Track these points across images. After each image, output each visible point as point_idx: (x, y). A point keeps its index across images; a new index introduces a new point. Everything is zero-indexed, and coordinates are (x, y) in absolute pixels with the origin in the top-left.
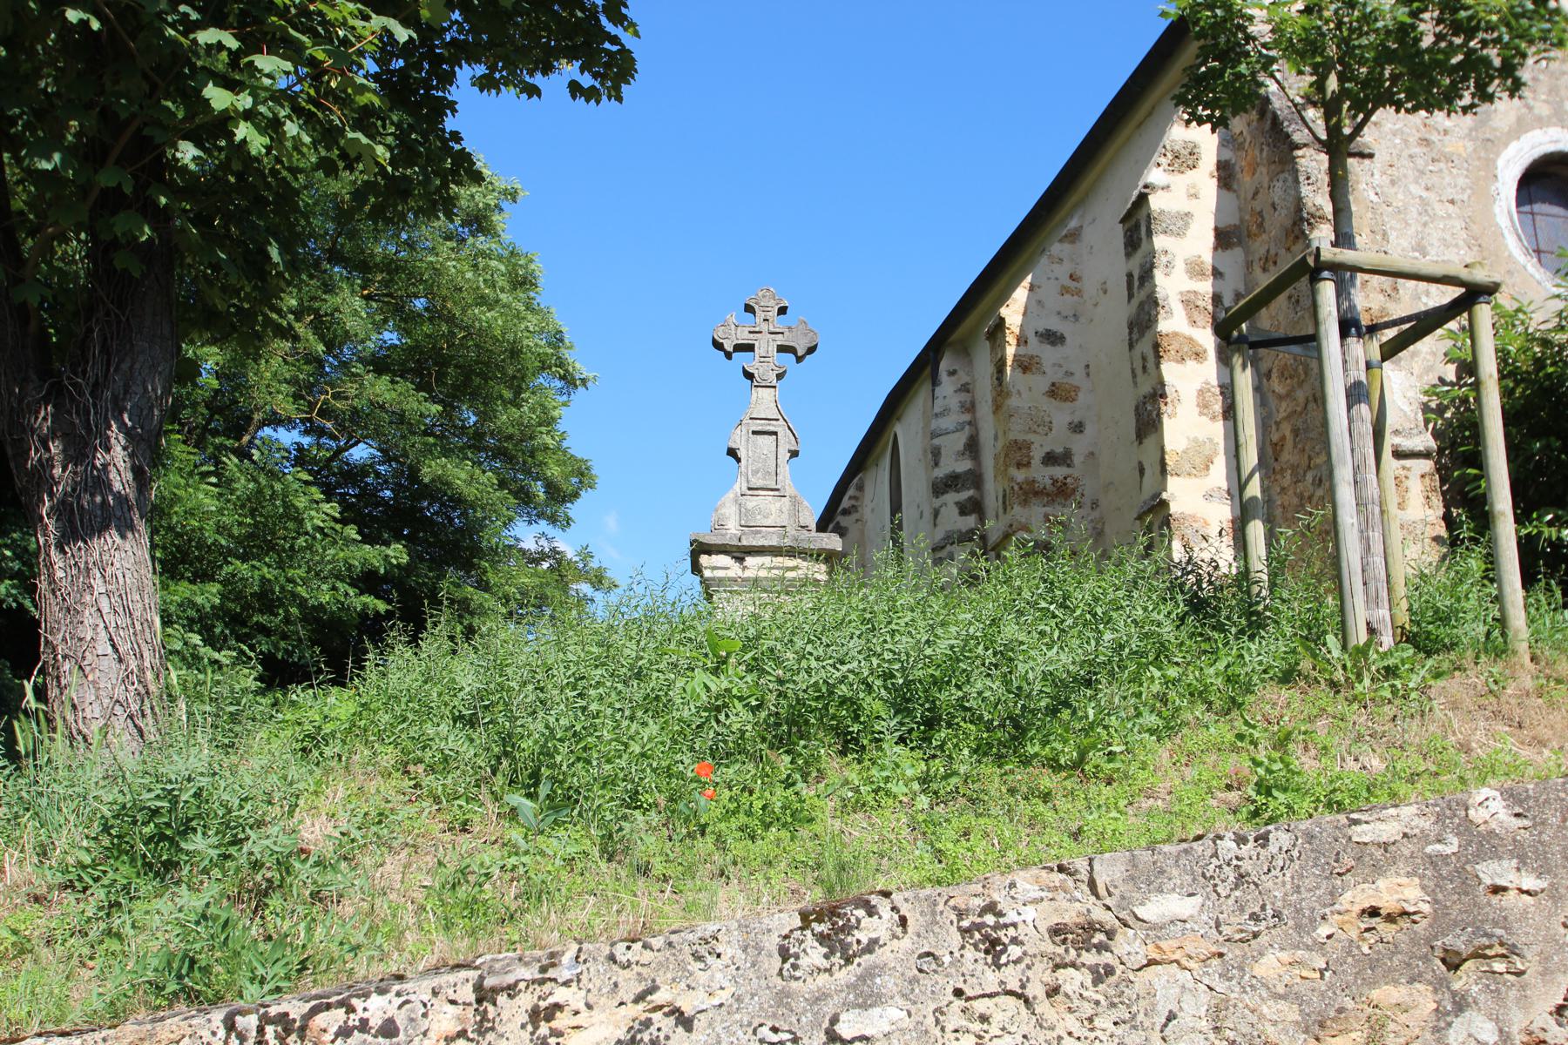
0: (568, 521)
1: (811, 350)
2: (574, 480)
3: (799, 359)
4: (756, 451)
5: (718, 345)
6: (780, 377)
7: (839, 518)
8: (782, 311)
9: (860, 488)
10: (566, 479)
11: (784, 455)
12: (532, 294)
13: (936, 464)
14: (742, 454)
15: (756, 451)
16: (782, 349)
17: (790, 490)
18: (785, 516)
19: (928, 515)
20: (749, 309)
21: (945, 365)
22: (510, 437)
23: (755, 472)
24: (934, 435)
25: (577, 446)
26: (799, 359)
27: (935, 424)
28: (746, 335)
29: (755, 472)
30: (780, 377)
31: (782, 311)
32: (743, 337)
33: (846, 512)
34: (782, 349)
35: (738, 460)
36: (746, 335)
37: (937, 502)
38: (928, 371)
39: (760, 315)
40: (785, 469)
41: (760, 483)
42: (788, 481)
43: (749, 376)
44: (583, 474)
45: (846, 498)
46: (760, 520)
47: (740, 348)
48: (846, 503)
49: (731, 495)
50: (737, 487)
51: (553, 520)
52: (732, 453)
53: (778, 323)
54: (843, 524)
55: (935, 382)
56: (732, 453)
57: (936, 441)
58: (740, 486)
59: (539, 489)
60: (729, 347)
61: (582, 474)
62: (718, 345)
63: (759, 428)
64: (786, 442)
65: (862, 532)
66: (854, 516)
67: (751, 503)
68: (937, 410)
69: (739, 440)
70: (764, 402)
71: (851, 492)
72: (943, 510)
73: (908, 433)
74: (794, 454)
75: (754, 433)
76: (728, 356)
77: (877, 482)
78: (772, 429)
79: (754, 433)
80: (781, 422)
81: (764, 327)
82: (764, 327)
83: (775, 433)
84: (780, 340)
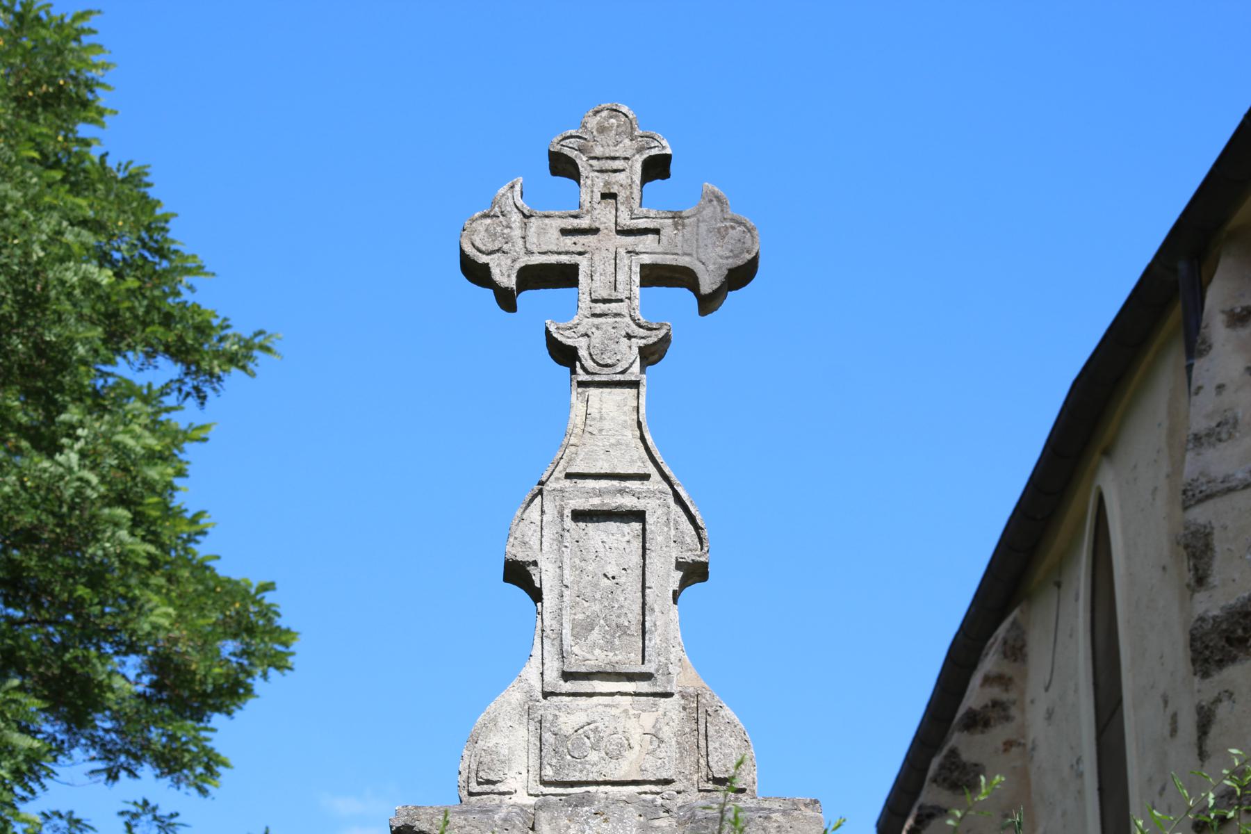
0: (212, 763)
1: (741, 276)
2: (229, 647)
3: (708, 304)
4: (588, 568)
5: (476, 273)
6: (650, 355)
7: (957, 739)
8: (657, 168)
9: (1016, 651)
10: (205, 643)
11: (665, 578)
12: (83, 130)
13: (1201, 580)
14: (545, 577)
15: (588, 568)
16: (654, 276)
17: (683, 677)
18: (670, 751)
19: (1188, 724)
20: (562, 166)
21: (1219, 296)
22: (29, 537)
23: (583, 629)
24: (1192, 496)
25: (231, 553)
26: (708, 304)
27: (1192, 466)
28: (553, 239)
29: (583, 629)
30: (650, 355)
31: (657, 168)
32: (546, 243)
33: (976, 722)
34: (654, 276)
35: (537, 595)
36: (553, 239)
37: (1208, 689)
38: (1176, 315)
39: (594, 184)
40: (667, 620)
41: (598, 659)
42: (676, 653)
43: (564, 355)
44: (256, 632)
45: (976, 680)
46: (596, 765)
47: (534, 277)
48: (975, 696)
49: (514, 696)
50: (531, 672)
51: (170, 763)
52: (518, 574)
53: (647, 206)
54: (967, 756)
55: (1195, 346)
56: (518, 574)
57: (1200, 514)
58: (539, 669)
59: (128, 675)
60: (505, 276)
61: (251, 630)
62: (476, 273)
63: (594, 503)
64: (670, 541)
65: (1022, 777)
66: (1000, 733)
67: (572, 716)
68: (1199, 424)
69: (535, 535)
70: (606, 427)
71: (990, 663)
72: (1223, 710)
73: (1132, 493)
74: (694, 573)
75: (578, 516)
76: (507, 300)
77: (1058, 637)
78: (628, 502)
79: (578, 516)
80: (656, 482)
81: (604, 216)
82: (604, 216)
83: (639, 516)
84: (650, 251)
